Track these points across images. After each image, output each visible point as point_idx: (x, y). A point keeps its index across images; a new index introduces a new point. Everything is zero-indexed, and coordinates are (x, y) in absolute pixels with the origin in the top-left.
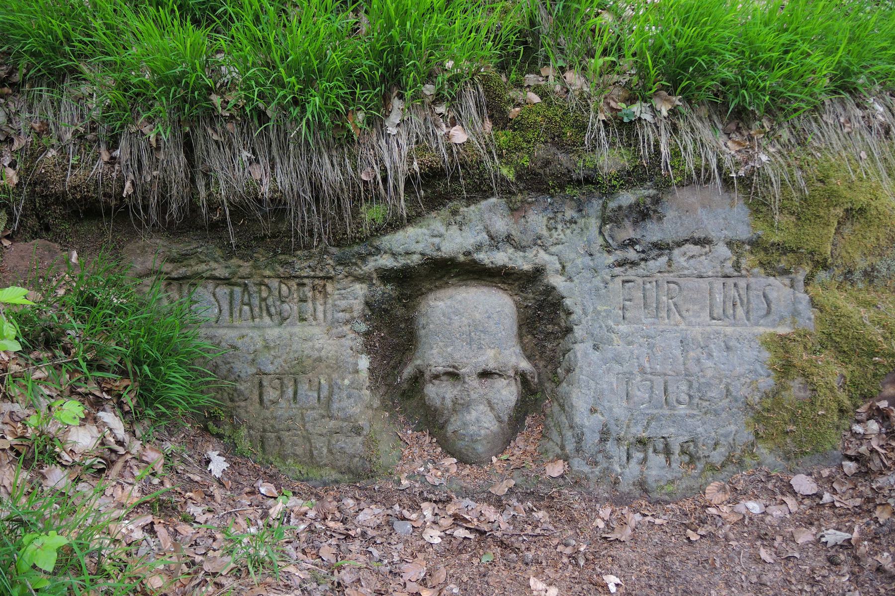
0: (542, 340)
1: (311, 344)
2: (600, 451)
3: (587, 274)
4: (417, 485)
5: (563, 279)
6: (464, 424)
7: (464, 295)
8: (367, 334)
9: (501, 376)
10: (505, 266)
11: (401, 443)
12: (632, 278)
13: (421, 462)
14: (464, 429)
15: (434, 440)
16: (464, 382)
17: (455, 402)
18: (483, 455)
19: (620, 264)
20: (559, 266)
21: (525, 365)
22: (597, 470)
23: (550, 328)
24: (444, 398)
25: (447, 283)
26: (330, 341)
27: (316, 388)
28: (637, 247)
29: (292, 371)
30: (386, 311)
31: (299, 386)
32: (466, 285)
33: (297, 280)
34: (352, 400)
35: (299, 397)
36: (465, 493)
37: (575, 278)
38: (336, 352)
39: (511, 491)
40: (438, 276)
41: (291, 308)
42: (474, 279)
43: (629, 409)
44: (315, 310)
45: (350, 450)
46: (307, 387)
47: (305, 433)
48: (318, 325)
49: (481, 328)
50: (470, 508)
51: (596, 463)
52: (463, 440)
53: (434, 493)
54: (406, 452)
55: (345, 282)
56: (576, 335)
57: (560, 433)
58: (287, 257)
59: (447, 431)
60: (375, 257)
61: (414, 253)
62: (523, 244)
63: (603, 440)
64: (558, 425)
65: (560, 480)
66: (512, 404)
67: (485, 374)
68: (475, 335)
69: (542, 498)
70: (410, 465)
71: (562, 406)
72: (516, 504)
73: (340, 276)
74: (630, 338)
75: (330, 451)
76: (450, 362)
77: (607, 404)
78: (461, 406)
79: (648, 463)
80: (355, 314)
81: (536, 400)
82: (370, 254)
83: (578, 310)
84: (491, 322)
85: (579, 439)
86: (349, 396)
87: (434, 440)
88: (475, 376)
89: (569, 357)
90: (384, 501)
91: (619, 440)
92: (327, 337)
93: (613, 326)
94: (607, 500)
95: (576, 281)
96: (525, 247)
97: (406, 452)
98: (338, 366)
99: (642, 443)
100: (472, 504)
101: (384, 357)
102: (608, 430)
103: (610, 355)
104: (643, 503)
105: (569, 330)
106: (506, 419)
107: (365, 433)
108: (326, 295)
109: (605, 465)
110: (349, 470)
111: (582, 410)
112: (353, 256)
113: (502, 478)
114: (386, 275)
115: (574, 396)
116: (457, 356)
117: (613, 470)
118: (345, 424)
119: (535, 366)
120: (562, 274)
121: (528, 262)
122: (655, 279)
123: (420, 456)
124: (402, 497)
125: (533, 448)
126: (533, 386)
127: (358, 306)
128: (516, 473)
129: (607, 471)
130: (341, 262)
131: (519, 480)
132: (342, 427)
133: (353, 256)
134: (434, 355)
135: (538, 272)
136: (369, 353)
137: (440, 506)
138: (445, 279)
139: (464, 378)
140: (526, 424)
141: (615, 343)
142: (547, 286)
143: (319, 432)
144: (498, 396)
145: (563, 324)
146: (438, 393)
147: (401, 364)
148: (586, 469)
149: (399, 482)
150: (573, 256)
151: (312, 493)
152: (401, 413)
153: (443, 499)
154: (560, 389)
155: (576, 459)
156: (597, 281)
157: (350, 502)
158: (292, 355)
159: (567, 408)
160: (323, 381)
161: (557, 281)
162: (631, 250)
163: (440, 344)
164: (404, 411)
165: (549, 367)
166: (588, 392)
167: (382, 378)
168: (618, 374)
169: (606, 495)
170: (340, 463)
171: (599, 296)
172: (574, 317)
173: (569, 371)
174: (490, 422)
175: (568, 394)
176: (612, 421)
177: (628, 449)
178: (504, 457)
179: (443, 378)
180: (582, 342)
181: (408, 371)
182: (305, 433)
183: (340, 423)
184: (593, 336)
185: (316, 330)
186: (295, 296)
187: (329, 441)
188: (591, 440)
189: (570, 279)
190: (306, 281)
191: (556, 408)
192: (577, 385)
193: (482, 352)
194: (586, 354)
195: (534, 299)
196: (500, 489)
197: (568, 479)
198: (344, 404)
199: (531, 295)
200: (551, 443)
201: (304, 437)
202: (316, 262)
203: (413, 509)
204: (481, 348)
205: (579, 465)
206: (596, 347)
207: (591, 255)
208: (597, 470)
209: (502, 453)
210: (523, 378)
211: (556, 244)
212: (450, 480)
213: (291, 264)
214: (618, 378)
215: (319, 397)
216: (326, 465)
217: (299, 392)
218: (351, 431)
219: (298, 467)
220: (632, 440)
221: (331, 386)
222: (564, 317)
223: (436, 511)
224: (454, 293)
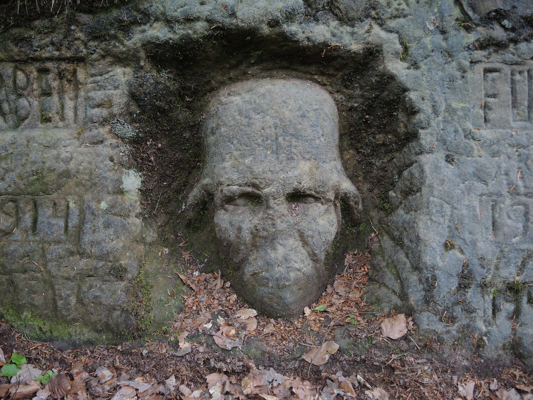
0: (368, 155)
1: (55, 152)
2: (457, 303)
3: (438, 58)
4: (201, 349)
5: (406, 65)
6: (268, 264)
7: (269, 86)
8: (135, 141)
9: (317, 199)
10: (325, 44)
11: (184, 288)
12: (498, 65)
13: (208, 315)
14: (267, 271)
15: (228, 284)
16: (268, 207)
17: (255, 234)
18: (293, 307)
19: (482, 45)
20: (399, 47)
21: (347, 186)
22: (454, 329)
23: (380, 138)
24: (240, 229)
25: (245, 73)
26: (82, 149)
27: (63, 214)
28: (505, 22)
29: (29, 190)
30: (163, 111)
31: (40, 212)
32: (271, 77)
33: (38, 65)
34: (111, 231)
35: (39, 226)
36: (269, 362)
37: (421, 64)
38: (90, 163)
39: (334, 359)
40: (233, 62)
41: (30, 103)
42: (283, 68)
43: (498, 244)
44: (63, 107)
45: (107, 300)
46: (50, 212)
47: (46, 277)
48: (67, 126)
49: (291, 131)
50: (275, 384)
51: (452, 319)
52: (266, 285)
53: (224, 361)
54: (190, 301)
55: (101, 65)
56: (423, 142)
57: (398, 276)
58: (22, 30)
59: (244, 273)
60: (143, 27)
61: (198, 19)
62: (352, 14)
63: (463, 287)
64: (394, 265)
65: (403, 343)
66: (331, 238)
67: (297, 197)
68: (284, 139)
69: (378, 369)
70: (194, 320)
71: (398, 242)
72: (342, 379)
73: (95, 56)
74: (495, 147)
75: (80, 301)
76: (249, 178)
77: (467, 236)
78: (263, 239)
79: (522, 318)
80: (116, 110)
81: (359, 232)
82: (135, 22)
83: (426, 107)
84: (306, 124)
85: (430, 285)
86: (107, 226)
87: (228, 284)
88: (283, 199)
89: (412, 174)
90: (155, 372)
91: (483, 286)
92: (77, 143)
93: (473, 130)
94: (467, 369)
95: (423, 67)
96: (353, 19)
97: (190, 301)
98: (93, 184)
99: (513, 289)
100: (279, 377)
101: (163, 177)
102: (470, 272)
103: (470, 170)
104: (518, 373)
105: (412, 136)
106: (322, 257)
107: (130, 276)
108: (77, 85)
109: (465, 322)
110: (108, 328)
111: (434, 245)
112: (111, 24)
113: (320, 339)
114: (160, 55)
115: (421, 225)
116: (258, 169)
117: (475, 329)
118: (101, 264)
119: (358, 189)
120: (403, 59)
121: (357, 42)
122: (526, 68)
123: (208, 307)
124: (180, 366)
125: (358, 295)
126: (357, 215)
127: (119, 98)
128: (338, 332)
129: (467, 330)
130: (96, 35)
131: (345, 343)
132: (96, 268)
133: (111, 24)
134: (227, 170)
135: (373, 53)
136: (140, 169)
137: (233, 379)
138: (243, 67)
139: (267, 201)
140: (346, 264)
141: (476, 153)
142: (383, 75)
143: (65, 275)
144: (313, 226)
145: (402, 129)
146: (235, 222)
147: (187, 185)
148: (440, 327)
149: (176, 345)
150: (419, 33)
151: (56, 359)
152: (186, 250)
153: (237, 369)
154: (394, 218)
155: (425, 314)
156: (452, 68)
157: (106, 373)
158: (28, 168)
159: (406, 241)
160: (72, 205)
161: (397, 67)
162: (497, 27)
163: (236, 153)
164: (189, 247)
165: (376, 191)
166: (441, 220)
167: (161, 203)
168: (482, 195)
169: (465, 363)
170: (94, 318)
171: (453, 89)
172: (420, 117)
173: (408, 192)
174: (302, 261)
175: (411, 226)
176: (476, 261)
177: (494, 299)
178: (320, 308)
179: (240, 201)
180: (431, 152)
181: (195, 194)
182: (46, 277)
183: (95, 263)
184: (445, 143)
185: (63, 134)
186: (35, 86)
187: (79, 288)
188: (446, 286)
189: (415, 65)
190: (49, 65)
191: (387, 243)
192: (425, 210)
193: (293, 164)
194: (437, 168)
195: (362, 96)
196: (318, 356)
197: (414, 342)
198: (101, 235)
199: (358, 92)
200: (384, 289)
201: (45, 282)
202: (61, 37)
203: (196, 383)
204: (292, 158)
205: (429, 322)
206: (449, 159)
207: (443, 32)
208: (454, 329)
209: (317, 301)
210: (344, 203)
211: (396, 17)
212: (247, 342)
213: (28, 41)
214: (481, 201)
215: (67, 226)
216: (75, 320)
217: (40, 219)
218: (109, 274)
219: (37, 323)
220: (500, 286)
221: (82, 212)
222: (404, 119)
223: (227, 389)
224: (254, 85)
